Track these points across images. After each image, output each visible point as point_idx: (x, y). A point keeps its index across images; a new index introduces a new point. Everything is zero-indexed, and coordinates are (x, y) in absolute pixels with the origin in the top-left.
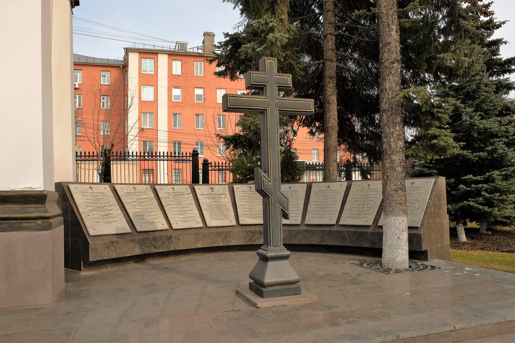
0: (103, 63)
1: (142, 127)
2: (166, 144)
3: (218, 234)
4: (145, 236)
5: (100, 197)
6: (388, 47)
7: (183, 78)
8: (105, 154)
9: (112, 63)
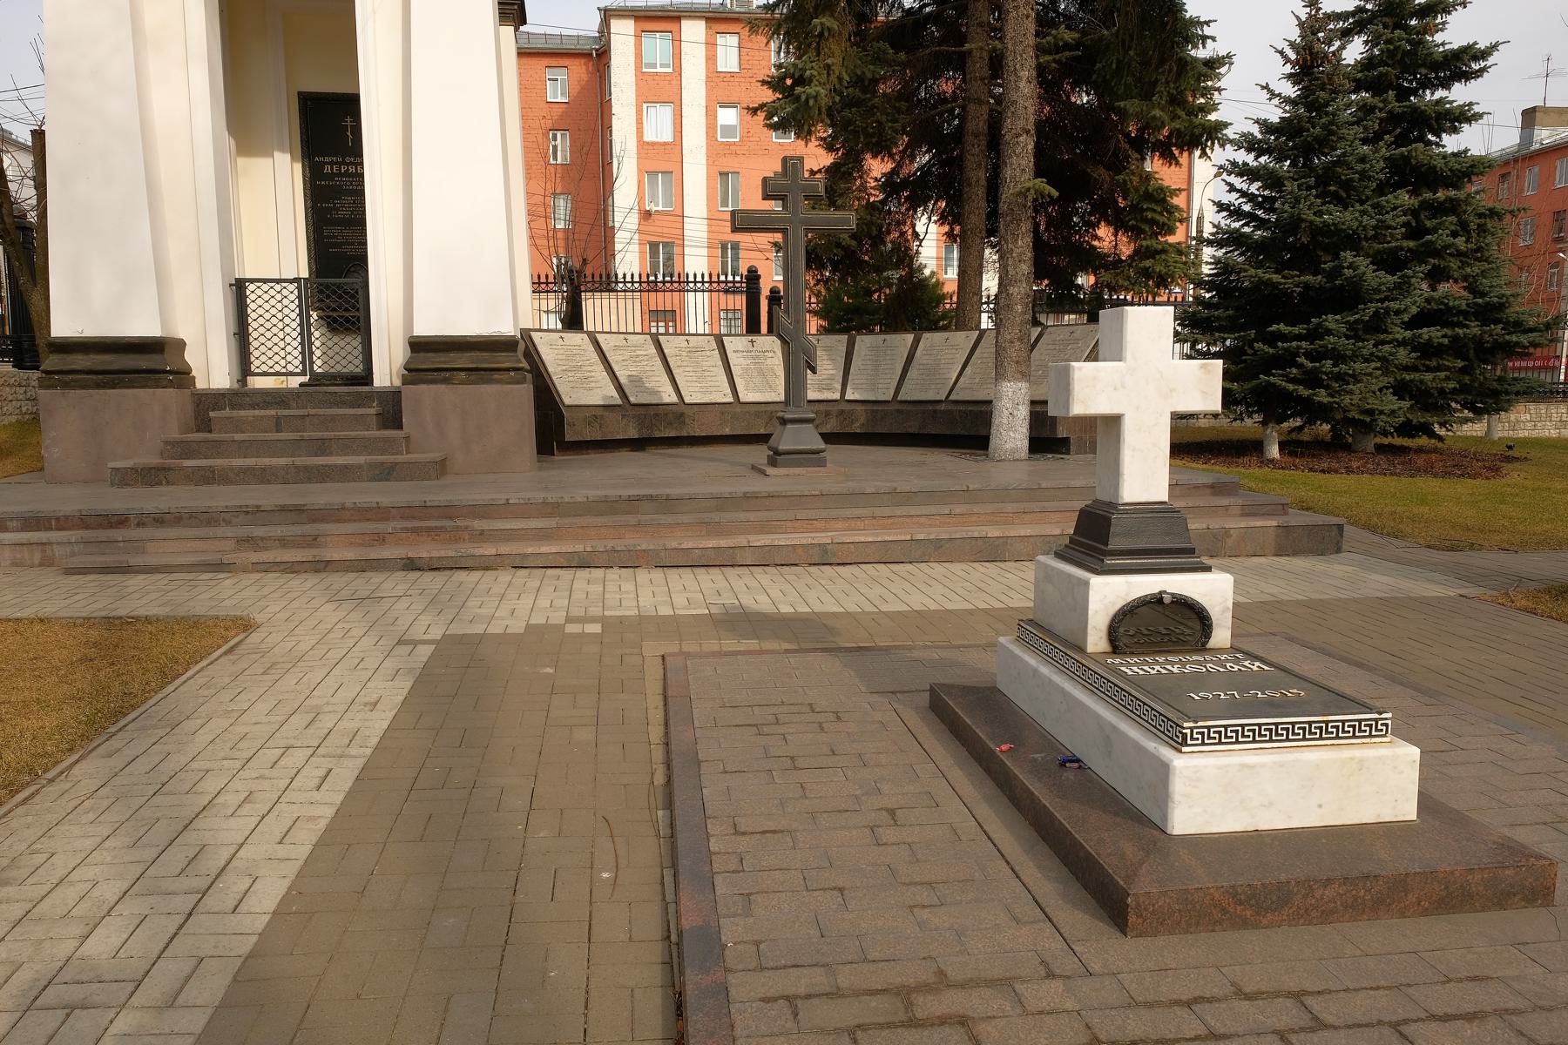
0: (551, 46)
1: (648, 208)
2: (705, 252)
3: (757, 415)
4: (642, 411)
5: (575, 352)
6: (1013, 109)
7: (743, 80)
8: (572, 280)
9: (570, 45)
